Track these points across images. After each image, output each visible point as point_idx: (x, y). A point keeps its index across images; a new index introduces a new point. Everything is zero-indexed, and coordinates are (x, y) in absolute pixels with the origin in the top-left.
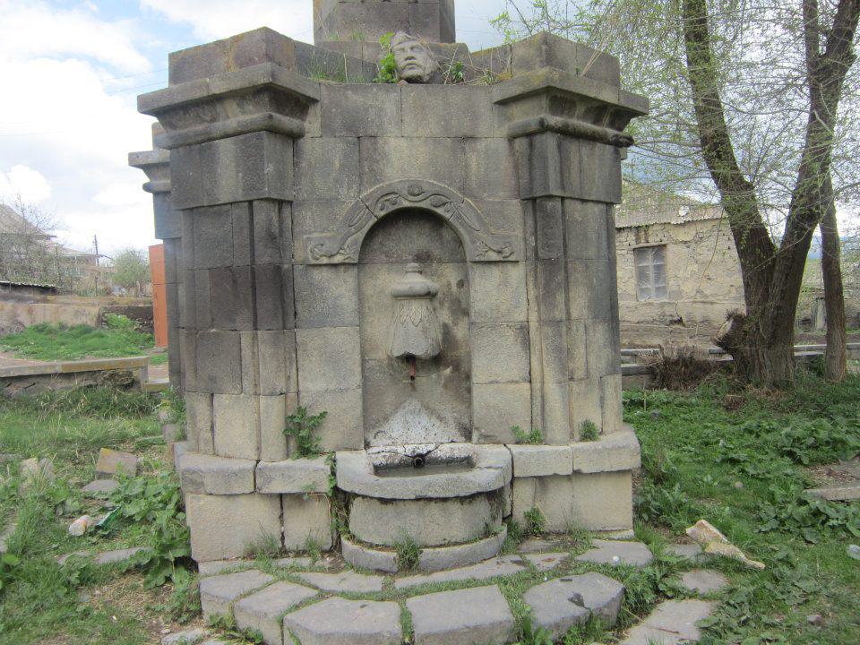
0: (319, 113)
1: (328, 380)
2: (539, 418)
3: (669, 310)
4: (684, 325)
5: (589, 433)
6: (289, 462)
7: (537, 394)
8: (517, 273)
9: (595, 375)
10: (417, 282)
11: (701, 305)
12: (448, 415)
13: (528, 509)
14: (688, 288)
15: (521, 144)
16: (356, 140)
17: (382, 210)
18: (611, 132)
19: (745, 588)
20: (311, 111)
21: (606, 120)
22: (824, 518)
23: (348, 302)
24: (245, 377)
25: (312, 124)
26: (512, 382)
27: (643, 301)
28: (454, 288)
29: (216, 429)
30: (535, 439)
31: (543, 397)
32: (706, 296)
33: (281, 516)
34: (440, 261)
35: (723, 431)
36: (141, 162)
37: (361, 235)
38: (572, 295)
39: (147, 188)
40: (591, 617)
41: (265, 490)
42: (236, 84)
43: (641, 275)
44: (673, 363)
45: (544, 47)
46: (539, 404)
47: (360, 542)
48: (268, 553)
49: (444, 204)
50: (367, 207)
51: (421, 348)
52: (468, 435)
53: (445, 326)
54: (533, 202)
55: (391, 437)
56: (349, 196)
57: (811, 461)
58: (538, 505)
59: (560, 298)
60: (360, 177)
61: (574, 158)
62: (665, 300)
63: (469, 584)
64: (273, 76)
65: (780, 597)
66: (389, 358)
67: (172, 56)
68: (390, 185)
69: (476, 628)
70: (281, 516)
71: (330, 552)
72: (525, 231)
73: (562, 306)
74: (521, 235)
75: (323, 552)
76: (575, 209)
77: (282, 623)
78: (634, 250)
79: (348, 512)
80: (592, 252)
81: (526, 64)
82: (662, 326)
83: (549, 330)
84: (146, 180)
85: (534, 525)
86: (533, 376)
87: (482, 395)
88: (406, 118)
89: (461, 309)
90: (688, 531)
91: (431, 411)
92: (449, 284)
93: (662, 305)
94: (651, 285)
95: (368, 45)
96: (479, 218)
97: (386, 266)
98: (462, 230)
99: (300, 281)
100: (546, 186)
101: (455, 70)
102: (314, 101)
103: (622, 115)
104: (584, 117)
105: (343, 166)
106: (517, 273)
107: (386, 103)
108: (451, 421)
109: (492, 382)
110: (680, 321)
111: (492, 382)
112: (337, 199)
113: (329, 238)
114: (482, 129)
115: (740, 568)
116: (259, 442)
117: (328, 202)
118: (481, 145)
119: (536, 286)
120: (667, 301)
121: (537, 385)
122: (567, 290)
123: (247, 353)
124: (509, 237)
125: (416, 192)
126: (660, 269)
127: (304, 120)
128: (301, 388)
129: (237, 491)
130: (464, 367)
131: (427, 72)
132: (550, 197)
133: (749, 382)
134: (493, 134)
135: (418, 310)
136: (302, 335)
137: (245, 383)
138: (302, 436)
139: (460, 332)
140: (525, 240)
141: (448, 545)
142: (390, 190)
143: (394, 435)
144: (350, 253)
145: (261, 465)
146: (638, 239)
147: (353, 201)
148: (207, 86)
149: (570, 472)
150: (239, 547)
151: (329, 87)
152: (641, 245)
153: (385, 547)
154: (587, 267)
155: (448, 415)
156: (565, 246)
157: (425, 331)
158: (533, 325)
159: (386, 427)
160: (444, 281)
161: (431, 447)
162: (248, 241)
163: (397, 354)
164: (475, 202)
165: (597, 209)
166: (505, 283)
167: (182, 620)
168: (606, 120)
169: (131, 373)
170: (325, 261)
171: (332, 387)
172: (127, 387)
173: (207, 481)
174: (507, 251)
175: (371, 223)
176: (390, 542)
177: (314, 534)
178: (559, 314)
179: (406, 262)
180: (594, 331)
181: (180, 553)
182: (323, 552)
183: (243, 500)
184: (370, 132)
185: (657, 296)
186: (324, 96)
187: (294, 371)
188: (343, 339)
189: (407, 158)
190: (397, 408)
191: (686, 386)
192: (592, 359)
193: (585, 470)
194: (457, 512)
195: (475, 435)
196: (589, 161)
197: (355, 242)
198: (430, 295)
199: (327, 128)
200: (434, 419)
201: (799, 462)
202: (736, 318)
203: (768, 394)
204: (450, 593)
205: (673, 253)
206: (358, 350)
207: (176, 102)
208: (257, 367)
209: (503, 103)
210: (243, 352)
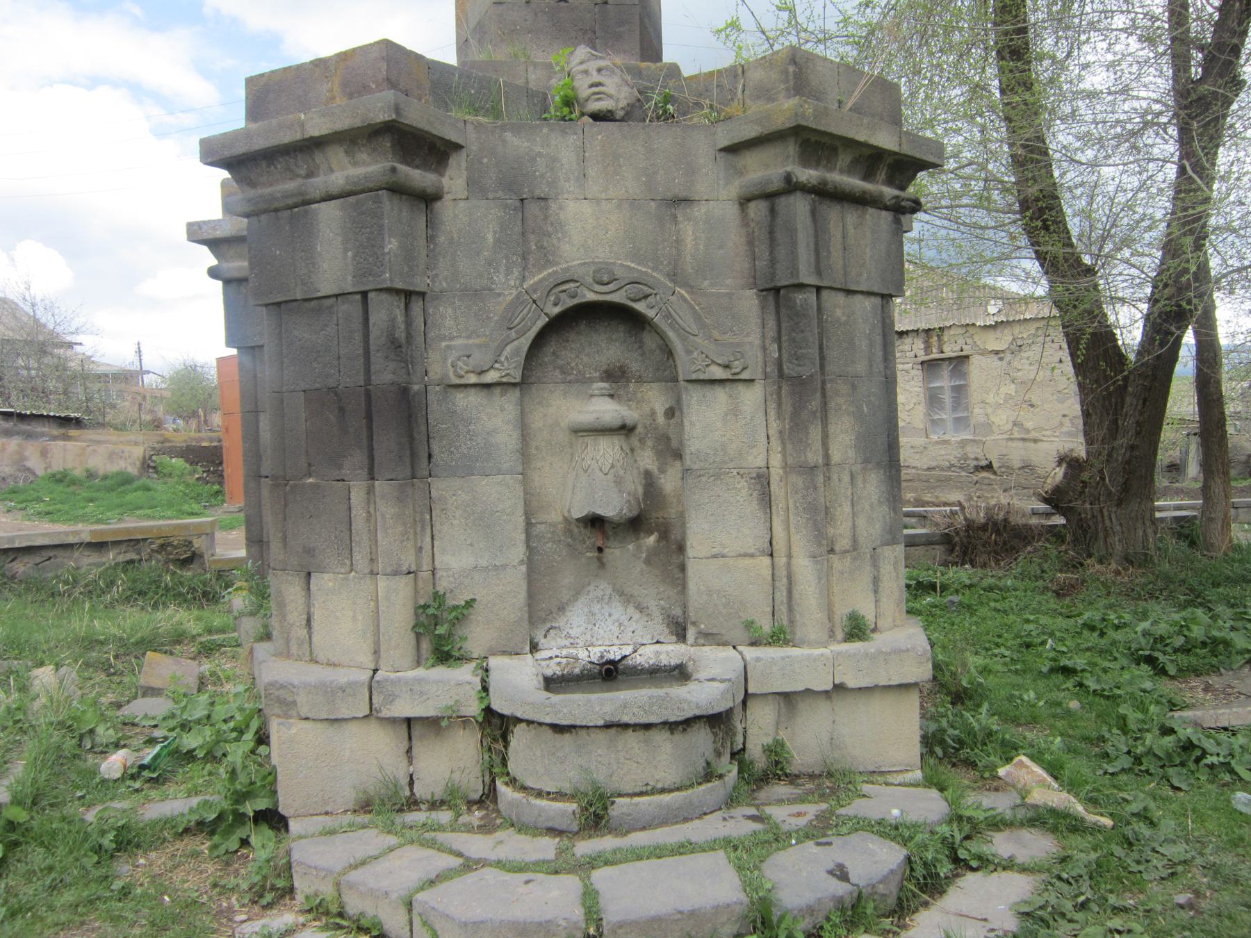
0: (464, 165)
2: (784, 609)
3: (973, 451)
4: (995, 473)
5: (856, 630)
6: (420, 672)
8: (752, 398)
10: (605, 410)
11: (1020, 444)
12: (653, 605)
13: (768, 740)
14: (1002, 419)
15: (758, 209)
16: (518, 204)
17: (556, 304)
18: (889, 192)
19: (1083, 854)
20: (452, 161)
21: (882, 175)
22: (1198, 753)
25: (454, 180)
26: (745, 555)
27: (934, 437)
29: (315, 624)
30: (779, 637)
31: (789, 577)
32: (1028, 431)
33: (409, 750)
34: (640, 380)
36: (205, 236)
38: (832, 428)
39: (213, 273)
40: (859, 897)
41: (385, 713)
42: (343, 123)
43: (933, 399)
44: (979, 528)
45: (791, 69)
46: (784, 587)
47: (524, 788)
49: (646, 297)
50: (534, 302)
51: (612, 507)
52: (679, 631)
53: (648, 474)
54: (776, 294)
55: (568, 636)
56: (508, 286)
57: (1180, 670)
58: (783, 735)
59: (815, 433)
62: (966, 436)
64: (397, 109)
65: (1135, 868)
66: (566, 520)
67: (250, 82)
68: (567, 269)
69: (692, 913)
70: (409, 750)
71: (480, 803)
72: (763, 336)
73: (817, 445)
75: (471, 803)
76: (836, 304)
77: (409, 906)
78: (922, 363)
80: (861, 367)
81: (765, 93)
82: (964, 474)
83: (799, 481)
84: (213, 261)
85: (777, 763)
86: (775, 547)
87: (702, 575)
88: (591, 172)
89: (671, 450)
90: (1002, 772)
91: (627, 598)
92: (653, 413)
93: (963, 444)
94: (946, 415)
96: (697, 318)
97: (562, 387)
98: (671, 335)
99: (436, 409)
100: (794, 271)
101: (662, 102)
102: (458, 147)
103: (904, 167)
105: (498, 241)
107: (561, 149)
109: (715, 556)
111: (715, 556)
112: (491, 290)
113: (479, 346)
114: (701, 189)
115: (1076, 826)
116: (377, 643)
118: (699, 211)
119: (779, 416)
121: (781, 561)
123: (358, 513)
124: (738, 345)
125: (605, 279)
126: (960, 392)
127: (442, 175)
130: (675, 535)
131: (621, 105)
132: (801, 287)
134: (718, 196)
135: (607, 451)
136: (439, 487)
137: (357, 556)
139: (669, 482)
140: (764, 349)
142: (567, 276)
143: (573, 633)
145: (379, 676)
146: (928, 348)
147: (514, 292)
148: (302, 125)
149: (829, 687)
150: (347, 795)
151: (478, 126)
153: (560, 796)
154: (854, 387)
155: (653, 605)
156: (822, 358)
157: (618, 481)
158: (776, 473)
159: (561, 622)
160: (647, 409)
161: (627, 650)
162: (361, 351)
163: (577, 514)
164: (691, 293)
166: (734, 412)
167: (264, 902)
168: (882, 175)
169: (190, 542)
170: (473, 379)
173: (302, 699)
175: (540, 324)
176: (567, 788)
177: (456, 776)
178: (814, 456)
180: (865, 481)
181: (262, 804)
182: (471, 803)
183: (353, 727)
184: (538, 193)
185: (957, 430)
186: (470, 139)
187: (428, 539)
188: (499, 493)
189: (592, 231)
190: (577, 594)
192: (861, 522)
193: (851, 684)
195: (691, 633)
196: (858, 233)
197: (516, 352)
198: (625, 429)
199: (475, 186)
200: (631, 610)
201: (1162, 672)
203: (1117, 573)
204: (654, 861)
205: (979, 369)
206: (520, 510)
207: (257, 147)
209: (733, 149)
210: (354, 513)
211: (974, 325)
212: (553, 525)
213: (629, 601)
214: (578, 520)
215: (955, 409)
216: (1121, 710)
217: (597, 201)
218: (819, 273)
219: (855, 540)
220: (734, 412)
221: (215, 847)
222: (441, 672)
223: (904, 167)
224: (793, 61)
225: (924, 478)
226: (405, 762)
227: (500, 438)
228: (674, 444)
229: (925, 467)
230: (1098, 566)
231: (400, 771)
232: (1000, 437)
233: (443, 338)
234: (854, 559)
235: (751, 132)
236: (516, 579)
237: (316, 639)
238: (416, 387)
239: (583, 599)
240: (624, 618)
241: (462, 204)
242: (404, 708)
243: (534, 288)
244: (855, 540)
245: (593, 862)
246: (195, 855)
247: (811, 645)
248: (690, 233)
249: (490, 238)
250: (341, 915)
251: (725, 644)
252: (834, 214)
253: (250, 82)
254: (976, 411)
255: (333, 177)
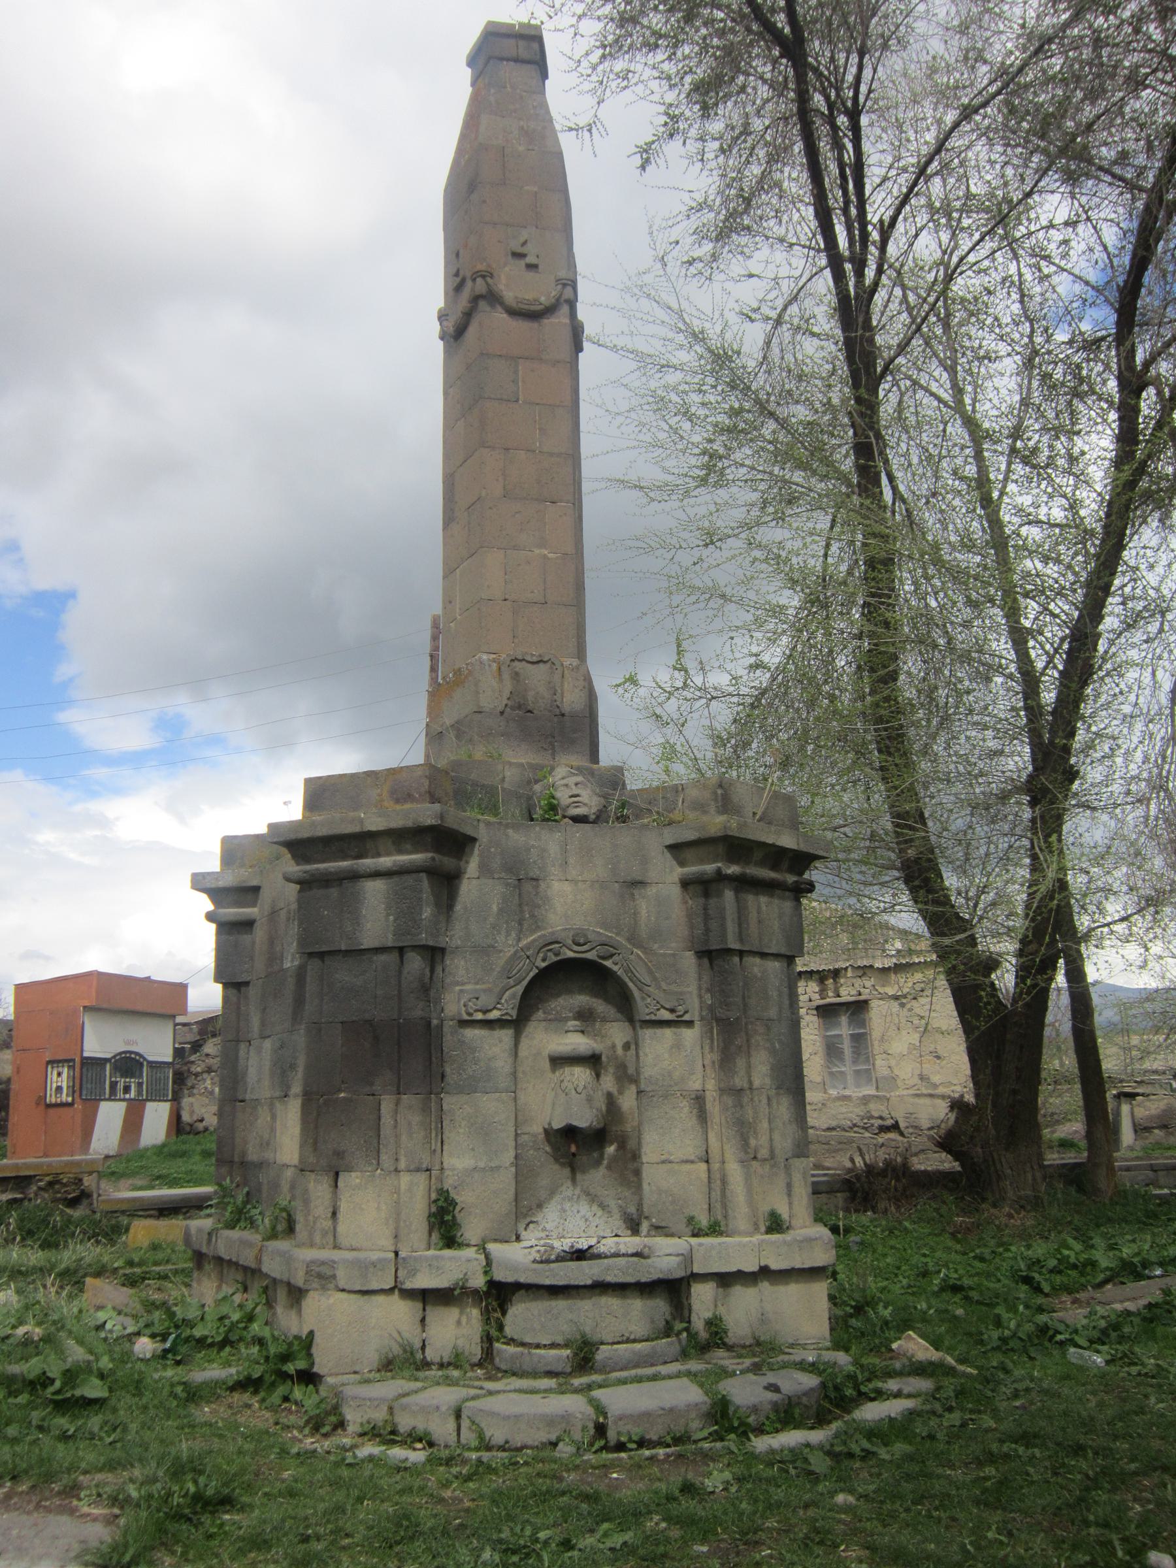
1: (475, 1160)
2: (718, 1206)
3: (876, 1108)
4: (902, 1134)
5: (775, 1225)
6: (431, 1252)
7: (717, 1176)
9: (780, 1157)
11: (928, 1101)
12: (612, 1204)
13: (708, 1315)
14: (907, 1072)
17: (544, 960)
18: (791, 879)
19: (950, 1386)
21: (785, 865)
22: (1051, 1333)
23: (503, 1064)
24: (383, 1150)
26: (687, 1161)
27: (833, 1092)
28: (620, 1051)
29: (340, 1216)
30: (714, 1229)
32: (935, 1086)
33: (423, 1320)
34: (604, 1020)
35: (949, 1261)
36: (208, 885)
37: (520, 989)
38: (753, 1060)
39: (210, 917)
40: (790, 1403)
41: (408, 1285)
42: (397, 823)
43: (832, 1050)
44: (879, 1174)
45: (719, 791)
46: (717, 1185)
47: (523, 1344)
48: (407, 1361)
49: (612, 956)
51: (584, 1119)
52: (634, 1227)
53: (609, 1096)
54: (711, 955)
55: (544, 1229)
56: (507, 945)
57: (1053, 1288)
58: (722, 1310)
59: (741, 1063)
60: (520, 924)
61: (753, 916)
62: (871, 1091)
63: (654, 1378)
64: (442, 817)
65: (989, 1394)
67: (309, 782)
68: (553, 933)
69: (671, 1410)
70: (423, 1320)
71: (480, 1365)
72: (700, 988)
73: (742, 1073)
74: (695, 992)
75: (473, 1366)
76: (755, 965)
77: (458, 1415)
78: (818, 1008)
79: (504, 1313)
80: (773, 1013)
81: (700, 807)
82: (867, 1135)
83: (729, 1101)
84: (210, 907)
85: (717, 1333)
87: (654, 1177)
88: (571, 861)
89: (627, 1076)
90: (894, 1346)
91: (592, 1198)
92: (614, 1046)
93: (866, 1100)
94: (847, 1068)
95: (510, 764)
96: (650, 972)
98: (630, 984)
99: (448, 1039)
100: (723, 936)
101: (618, 807)
103: (801, 860)
104: (762, 863)
105: (501, 910)
106: (690, 1036)
107: (548, 843)
108: (615, 1211)
109: (663, 1162)
110: (895, 1127)
111: (663, 1162)
113: (484, 991)
114: (652, 875)
115: (950, 1371)
117: (485, 951)
118: (651, 891)
120: (873, 1092)
121: (716, 1166)
122: (749, 1055)
123: (387, 1120)
124: (681, 993)
126: (860, 1040)
128: (445, 1165)
129: (375, 1286)
130: (631, 1144)
133: (984, 1200)
134: (666, 878)
135: (580, 1075)
136: (450, 1102)
137: (383, 1157)
138: (444, 1224)
139: (628, 1101)
140: (700, 997)
141: (628, 1341)
142: (553, 939)
143: (548, 1226)
144: (508, 1007)
146: (823, 993)
147: (512, 950)
148: (361, 821)
149: (755, 1268)
150: (371, 1357)
151: (488, 824)
152: (828, 1000)
153: (553, 1346)
154: (768, 1029)
155: (612, 1204)
157: (589, 1100)
158: (711, 1095)
160: (609, 1043)
161: (593, 1241)
163: (557, 1125)
164: (645, 953)
165: (775, 966)
166: (678, 1046)
168: (785, 865)
169: (81, 1180)
170: (479, 1016)
171: (481, 1164)
172: (73, 1203)
174: (681, 1009)
175: (532, 974)
176: (559, 1340)
177: (460, 1342)
178: (739, 1081)
179: (567, 1019)
180: (778, 1103)
181: (301, 1364)
182: (473, 1366)
183: (380, 1299)
184: (531, 874)
185: (858, 1086)
188: (493, 1106)
189: (572, 901)
190: (552, 1193)
191: (898, 1208)
192: (777, 1136)
193: (774, 1266)
194: (637, 1305)
196: (767, 911)
197: (513, 996)
198: (593, 1061)
199: (485, 870)
200: (595, 1208)
201: (1038, 1289)
202: (957, 1105)
203: (1010, 1216)
204: (636, 1385)
205: (878, 1012)
206: (512, 1123)
208: (397, 1136)
209: (676, 849)
211: (871, 967)
212: (534, 1135)
213: (593, 1201)
214: (558, 1130)
215: (855, 1062)
216: (997, 1311)
217: (574, 881)
218: (741, 940)
219: (772, 1151)
220: (678, 1046)
221: (263, 1400)
222: (447, 1252)
223: (801, 860)
224: (720, 786)
225: (823, 1140)
226: (419, 1329)
227: (499, 1064)
228: (631, 1071)
229: (825, 1126)
230: (992, 1210)
231: (412, 1335)
232: (905, 1092)
233: (458, 984)
234: (772, 1166)
235: (691, 836)
236: (505, 1181)
237: (341, 1229)
238: (435, 1022)
239: (557, 1198)
240: (589, 1215)
241: (474, 882)
242: (424, 1281)
243: (528, 947)
244: (772, 1151)
245: (590, 1387)
246: (248, 1406)
247: (740, 1234)
248: (644, 908)
249: (495, 908)
250: (393, 1432)
251: (672, 1235)
252: (750, 899)
253: (309, 782)
254: (879, 1062)
255: (382, 860)
